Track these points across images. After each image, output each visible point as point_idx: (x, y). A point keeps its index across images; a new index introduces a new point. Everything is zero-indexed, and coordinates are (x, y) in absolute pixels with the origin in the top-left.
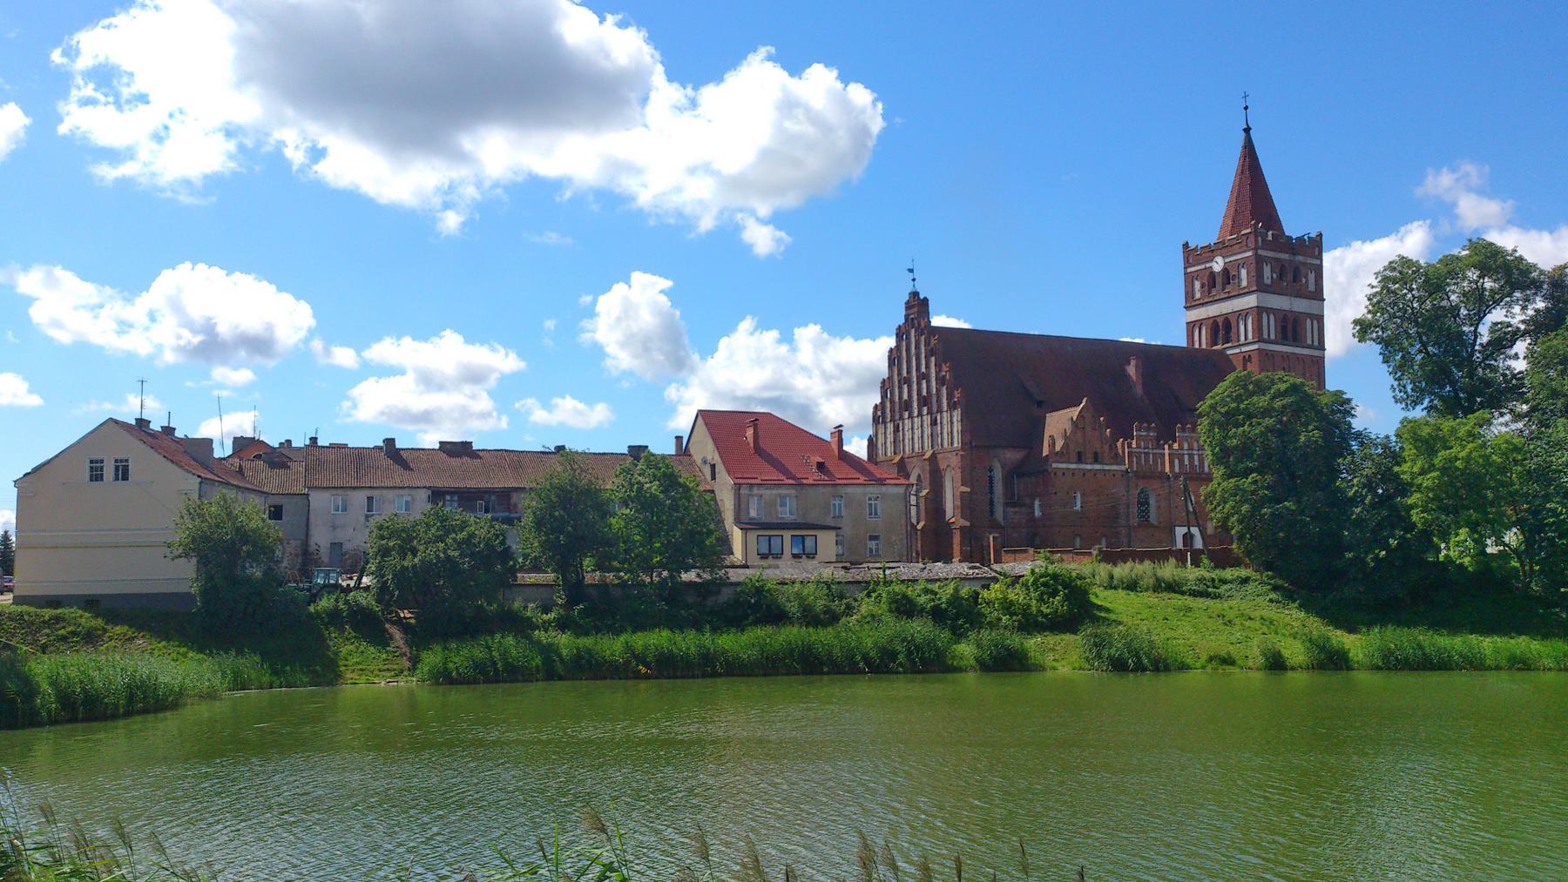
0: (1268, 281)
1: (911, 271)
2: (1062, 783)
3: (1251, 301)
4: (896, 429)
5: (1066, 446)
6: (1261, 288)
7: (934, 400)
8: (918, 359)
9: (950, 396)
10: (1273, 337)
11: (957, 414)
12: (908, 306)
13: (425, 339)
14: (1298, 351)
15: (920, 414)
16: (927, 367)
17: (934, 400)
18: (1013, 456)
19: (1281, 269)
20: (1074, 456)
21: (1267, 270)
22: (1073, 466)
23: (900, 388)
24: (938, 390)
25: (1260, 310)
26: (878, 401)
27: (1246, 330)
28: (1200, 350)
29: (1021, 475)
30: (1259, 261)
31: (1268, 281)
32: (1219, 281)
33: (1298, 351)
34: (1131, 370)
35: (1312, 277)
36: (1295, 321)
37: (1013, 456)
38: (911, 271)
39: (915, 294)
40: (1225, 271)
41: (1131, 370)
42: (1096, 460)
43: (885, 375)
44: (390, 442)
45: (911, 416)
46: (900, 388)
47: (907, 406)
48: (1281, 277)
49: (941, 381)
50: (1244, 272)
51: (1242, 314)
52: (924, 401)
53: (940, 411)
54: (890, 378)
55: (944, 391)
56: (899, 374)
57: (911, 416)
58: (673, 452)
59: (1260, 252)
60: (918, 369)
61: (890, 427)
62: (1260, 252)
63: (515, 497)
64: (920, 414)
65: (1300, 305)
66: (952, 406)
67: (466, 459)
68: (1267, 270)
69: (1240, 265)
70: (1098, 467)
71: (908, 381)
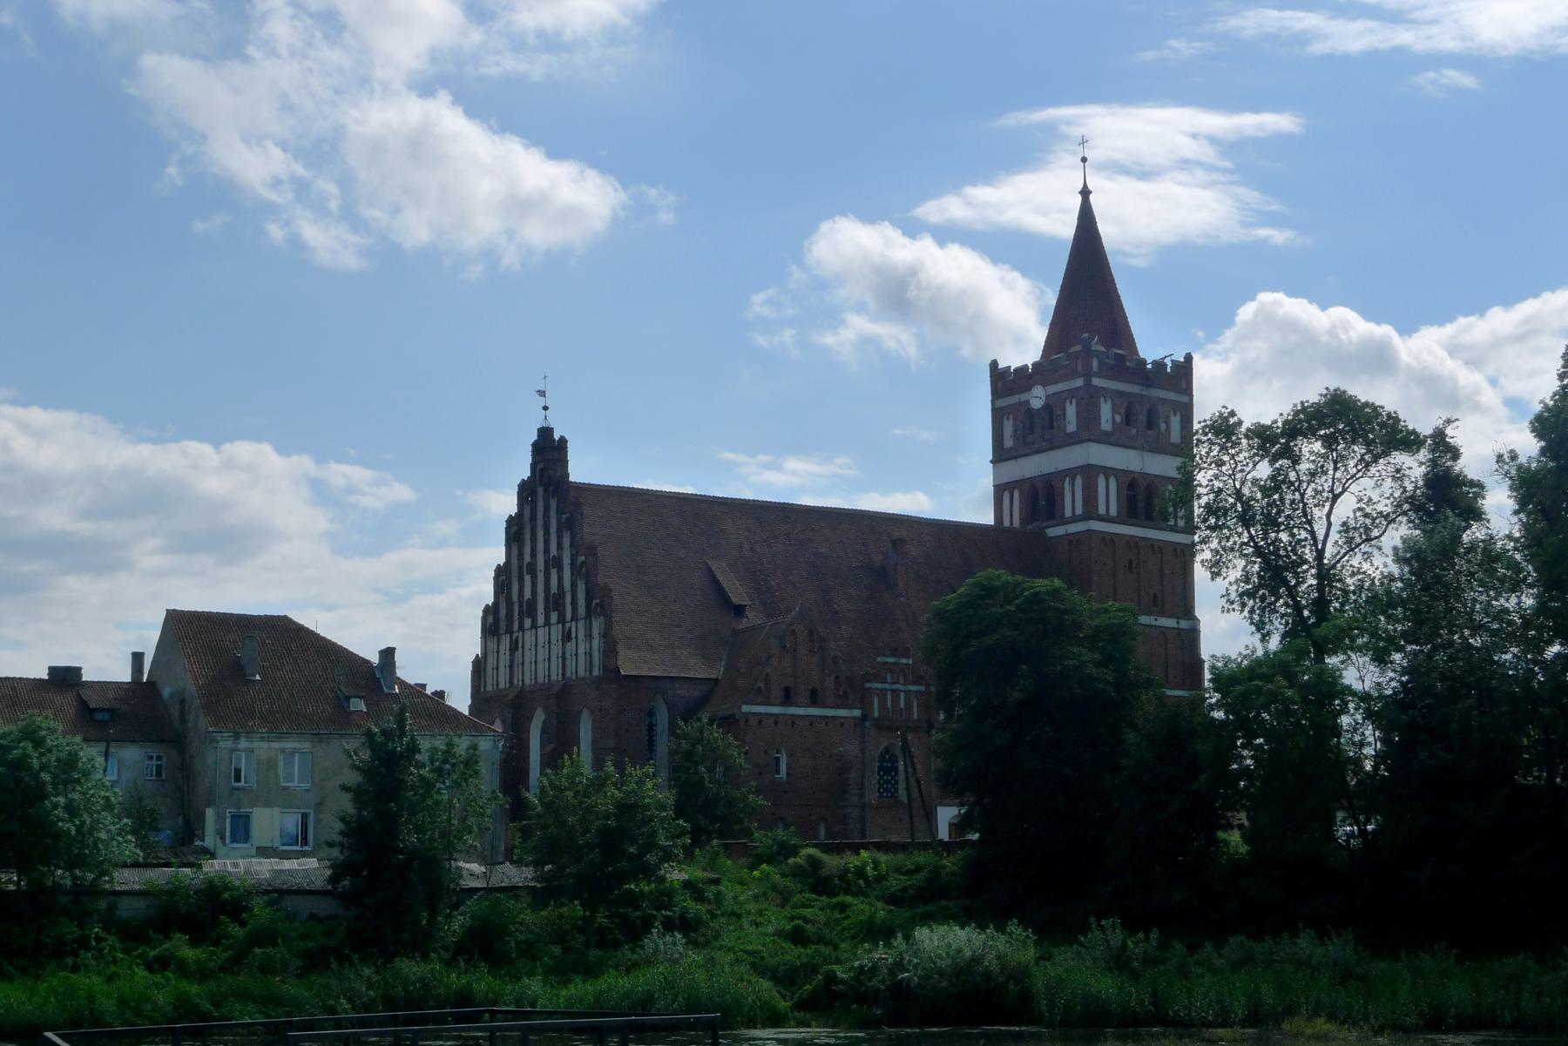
1: (542, 393)
4: (514, 647)
8: (546, 528)
16: (560, 547)
22: (801, 711)
39: (545, 433)
40: (1048, 408)
42: (814, 699)
45: (534, 626)
47: (530, 610)
50: (1071, 411)
52: (554, 602)
56: (547, 550)
57: (534, 626)
60: (547, 550)
64: (547, 623)
65: (1163, 466)
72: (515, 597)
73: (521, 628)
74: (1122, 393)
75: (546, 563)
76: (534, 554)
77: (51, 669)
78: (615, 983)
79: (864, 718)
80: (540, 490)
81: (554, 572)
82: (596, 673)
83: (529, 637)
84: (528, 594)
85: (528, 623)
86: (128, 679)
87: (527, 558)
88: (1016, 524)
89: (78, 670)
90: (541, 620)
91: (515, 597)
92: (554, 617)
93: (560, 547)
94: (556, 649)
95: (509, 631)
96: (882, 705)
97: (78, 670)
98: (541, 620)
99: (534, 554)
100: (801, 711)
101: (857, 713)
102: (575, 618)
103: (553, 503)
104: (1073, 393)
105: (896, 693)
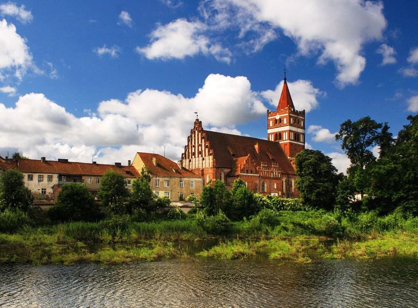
0: (292, 123)
1: (196, 113)
2: (241, 285)
3: (288, 128)
4: (190, 161)
5: (244, 168)
6: (291, 125)
7: (204, 152)
8: (198, 139)
9: (209, 151)
10: (287, 138)
11: (211, 157)
12: (195, 123)
13: (190, 98)
14: (299, 143)
15: (198, 157)
16: (201, 142)
17: (204, 152)
18: (227, 171)
19: (295, 119)
20: (246, 171)
21: (292, 119)
22: (250, 174)
23: (192, 148)
24: (205, 149)
25: (290, 131)
26: (184, 152)
27: (285, 136)
28: (271, 142)
29: (230, 177)
30: (290, 117)
31: (292, 123)
32: (278, 122)
33: (299, 143)
34: (256, 146)
35: (302, 122)
36: (298, 135)
37: (227, 171)
38: (196, 113)
39: (197, 120)
40: (280, 119)
41: (256, 146)
42: (251, 173)
43: (187, 144)
44: (44, 158)
45: (195, 157)
46: (192, 148)
47: (194, 154)
48: (295, 122)
49: (206, 147)
50: (285, 120)
51: (285, 131)
52: (200, 153)
53: (205, 156)
54: (188, 145)
55: (207, 150)
56: (191, 144)
57: (195, 157)
58: (127, 165)
59: (290, 114)
60: (198, 143)
61: (188, 160)
62: (290, 114)
63: (83, 178)
64: (198, 157)
65: (300, 130)
66: (210, 155)
67: (66, 164)
68: (292, 119)
69: (284, 117)
70: (252, 175)
71: (194, 146)
72: (190, 152)
73: (192, 158)
74: (294, 117)
75: (191, 147)
76: (195, 143)
77: (59, 159)
78: (329, 239)
79: (260, 176)
80: (196, 131)
81: (200, 147)
82: (210, 166)
83: (194, 159)
84: (193, 151)
85: (193, 157)
86: (127, 165)
87: (193, 144)
88: (273, 140)
89: (67, 160)
90: (197, 156)
91: (190, 152)
92: (200, 156)
93: (201, 142)
94: (201, 162)
95: (189, 158)
96: (262, 174)
97: (67, 160)
98: (197, 156)
99: (195, 143)
100: (250, 174)
101: (258, 175)
102: (205, 156)
103: (200, 134)
104: (285, 117)
105: (276, 172)
